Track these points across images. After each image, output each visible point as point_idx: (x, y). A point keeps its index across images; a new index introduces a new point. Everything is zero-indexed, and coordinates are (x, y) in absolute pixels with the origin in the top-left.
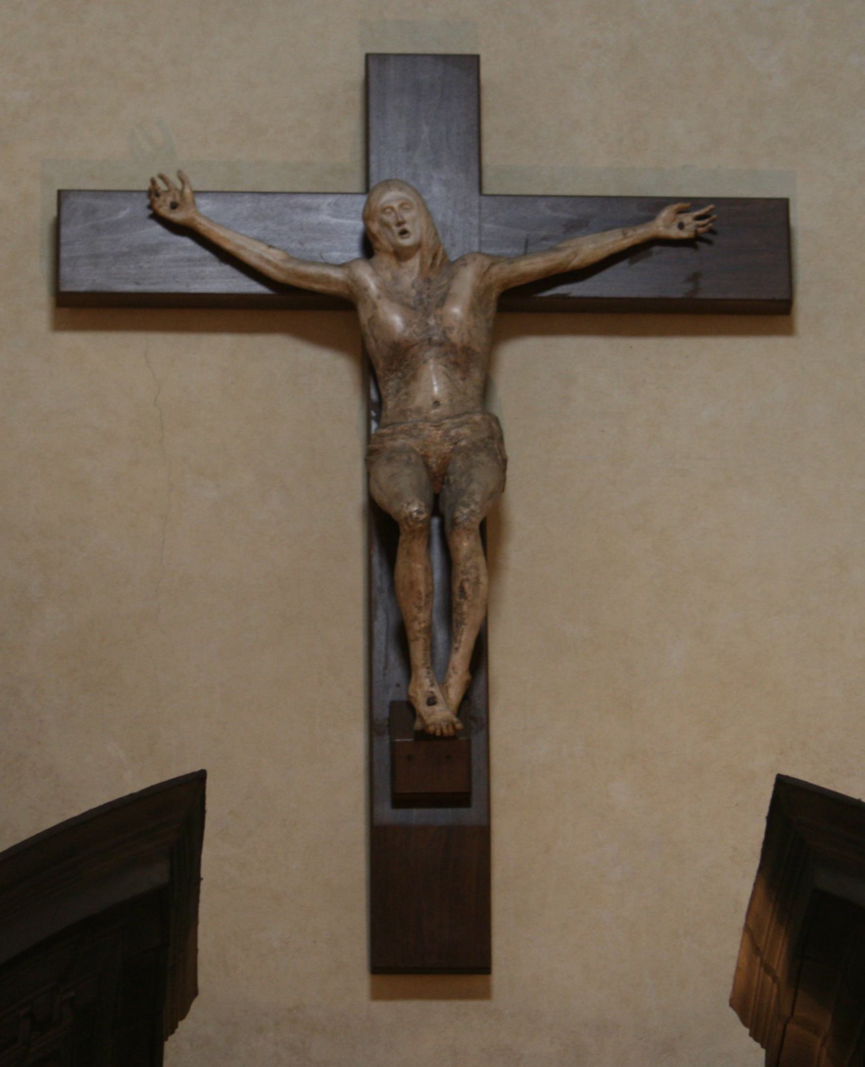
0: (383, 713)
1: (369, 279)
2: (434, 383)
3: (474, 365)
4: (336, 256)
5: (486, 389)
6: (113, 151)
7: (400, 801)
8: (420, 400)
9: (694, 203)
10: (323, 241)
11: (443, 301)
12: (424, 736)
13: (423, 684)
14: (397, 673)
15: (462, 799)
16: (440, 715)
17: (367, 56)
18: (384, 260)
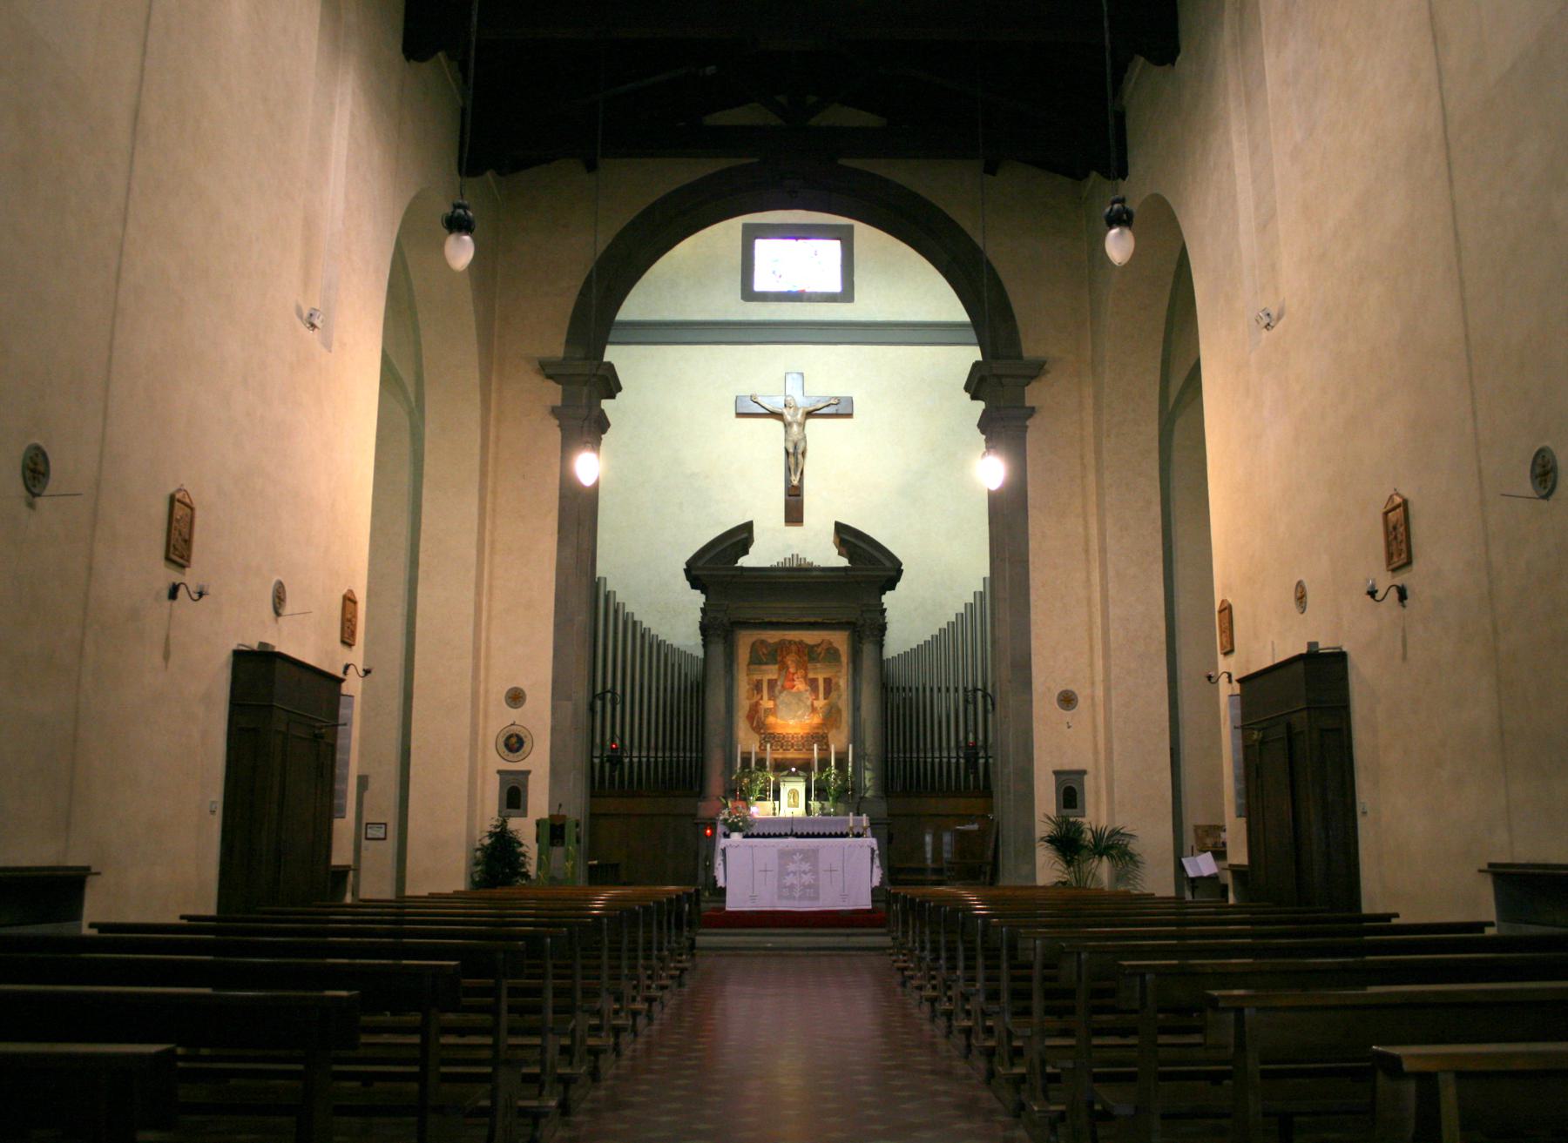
1: (785, 411)
2: (795, 428)
3: (802, 425)
10: (776, 404)
16: (795, 483)
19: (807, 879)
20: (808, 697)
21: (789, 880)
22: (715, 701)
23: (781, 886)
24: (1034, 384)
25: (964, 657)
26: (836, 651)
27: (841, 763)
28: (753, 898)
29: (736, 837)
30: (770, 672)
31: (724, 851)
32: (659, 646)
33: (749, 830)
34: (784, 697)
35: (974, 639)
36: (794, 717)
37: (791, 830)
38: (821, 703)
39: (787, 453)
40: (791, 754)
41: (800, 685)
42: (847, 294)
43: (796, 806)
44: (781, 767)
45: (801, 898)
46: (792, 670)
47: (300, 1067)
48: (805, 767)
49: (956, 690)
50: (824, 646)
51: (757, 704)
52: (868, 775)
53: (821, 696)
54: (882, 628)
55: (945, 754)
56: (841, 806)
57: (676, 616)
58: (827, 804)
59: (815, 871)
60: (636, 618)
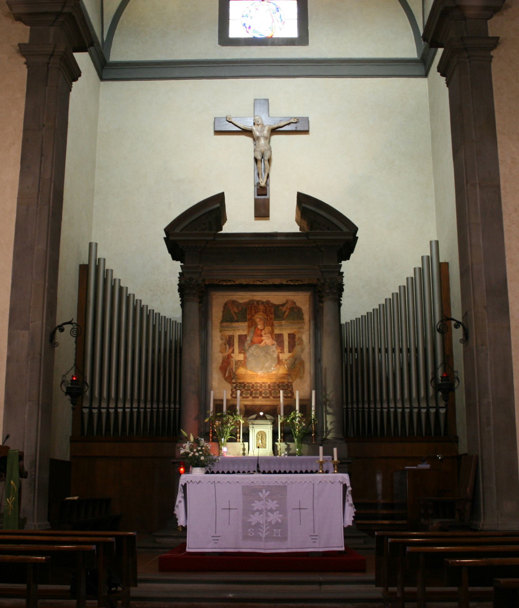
0: (256, 184)
1: (254, 128)
2: (262, 141)
3: (268, 139)
4: (250, 125)
5: (269, 142)
6: (222, 113)
7: (258, 195)
8: (261, 144)
9: (296, 118)
10: (248, 124)
11: (264, 130)
12: (261, 187)
13: (261, 180)
14: (258, 179)
15: (266, 195)
16: (263, 184)
17: (255, 100)
18: (256, 126)
19: (274, 517)
20: (274, 350)
21: (254, 519)
22: (192, 354)
23: (246, 525)
24: (495, 18)
25: (407, 317)
26: (299, 310)
27: (305, 408)
28: (216, 538)
29: (197, 472)
30: (241, 329)
31: (185, 487)
32: (142, 309)
33: (208, 464)
34: (253, 350)
35: (400, 328)
36: (262, 367)
37: (258, 466)
38: (286, 356)
39: (256, 160)
40: (260, 402)
41: (267, 340)
42: (303, 38)
43: (265, 447)
44: (250, 412)
45: (268, 538)
46: (260, 327)
47: (400, 435)
48: (272, 412)
49: (401, 351)
50: (289, 306)
51: (229, 357)
52: (329, 418)
53: (286, 349)
54: (340, 288)
55: (392, 405)
56: (305, 447)
57: (155, 280)
58: (292, 445)
59: (282, 509)
60: (109, 266)
